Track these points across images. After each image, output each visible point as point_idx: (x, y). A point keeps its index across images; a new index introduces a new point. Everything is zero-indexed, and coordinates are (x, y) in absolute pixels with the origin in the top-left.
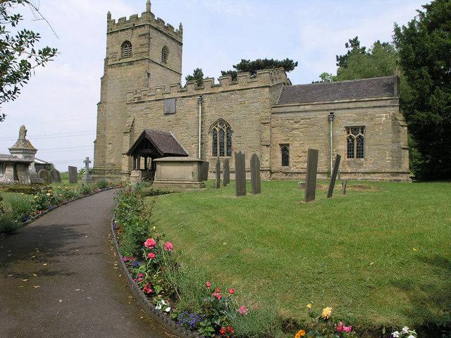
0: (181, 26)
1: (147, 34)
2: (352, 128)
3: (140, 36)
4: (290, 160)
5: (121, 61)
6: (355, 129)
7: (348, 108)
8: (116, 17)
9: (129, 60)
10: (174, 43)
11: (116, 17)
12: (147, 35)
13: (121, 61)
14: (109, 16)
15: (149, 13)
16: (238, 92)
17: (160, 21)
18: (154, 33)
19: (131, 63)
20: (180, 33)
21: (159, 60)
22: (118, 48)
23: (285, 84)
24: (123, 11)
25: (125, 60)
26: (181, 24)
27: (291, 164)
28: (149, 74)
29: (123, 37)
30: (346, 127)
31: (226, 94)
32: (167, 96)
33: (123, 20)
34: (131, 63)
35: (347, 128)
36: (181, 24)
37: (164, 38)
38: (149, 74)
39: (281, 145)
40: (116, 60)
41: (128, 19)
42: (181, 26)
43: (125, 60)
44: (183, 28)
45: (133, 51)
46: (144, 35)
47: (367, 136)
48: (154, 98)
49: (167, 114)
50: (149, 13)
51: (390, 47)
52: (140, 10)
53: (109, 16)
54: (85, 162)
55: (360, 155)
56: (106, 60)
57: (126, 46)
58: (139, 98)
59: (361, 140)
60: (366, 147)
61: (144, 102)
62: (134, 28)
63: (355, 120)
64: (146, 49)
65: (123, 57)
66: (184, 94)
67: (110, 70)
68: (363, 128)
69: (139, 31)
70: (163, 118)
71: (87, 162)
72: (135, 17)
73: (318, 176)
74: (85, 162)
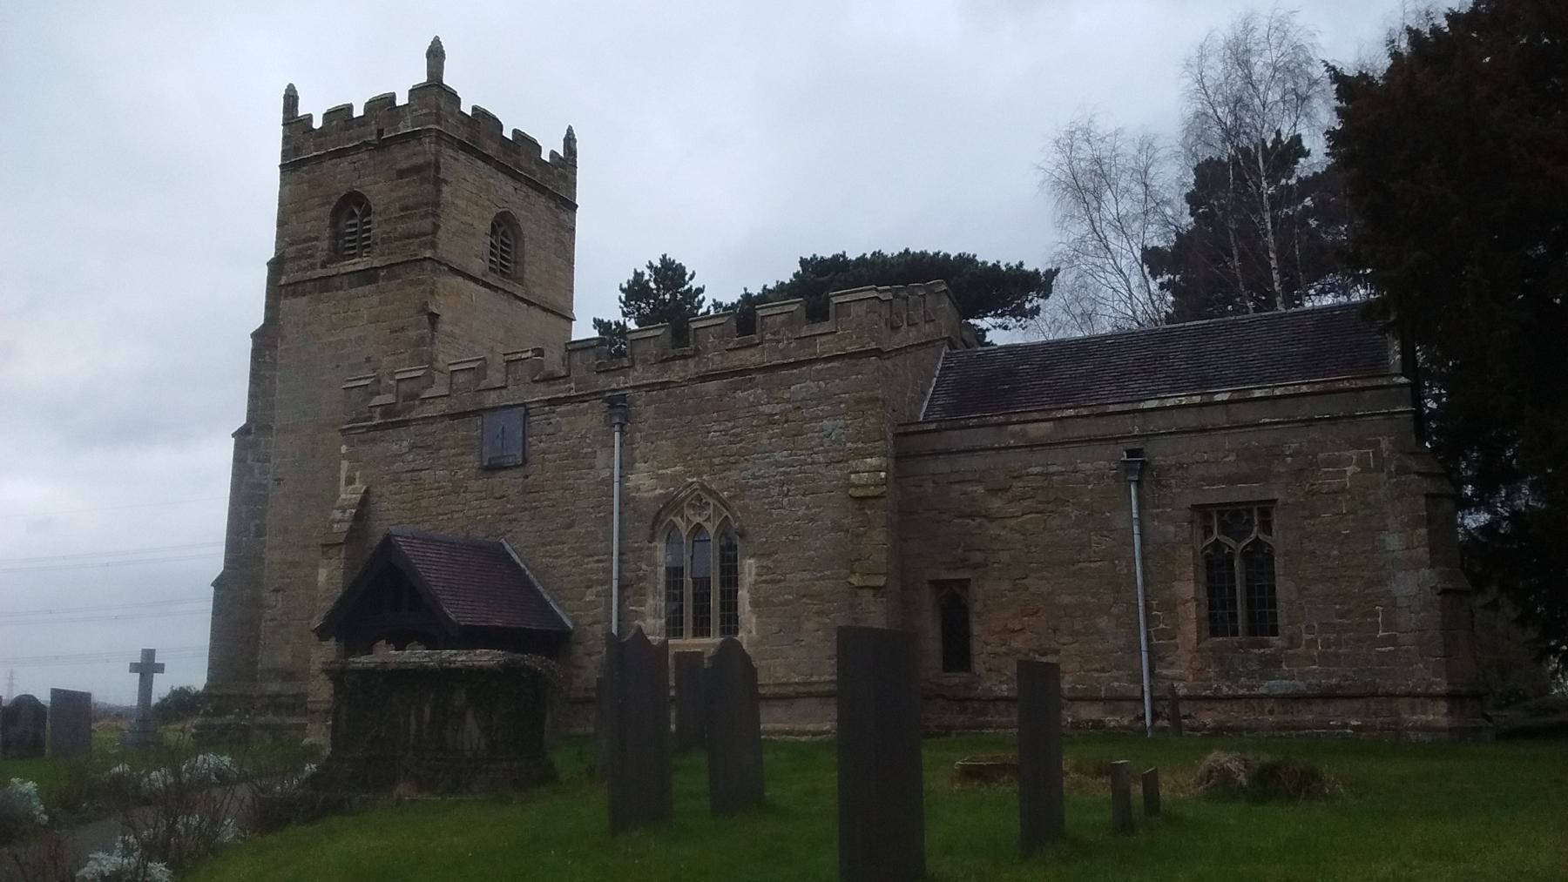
0: (570, 140)
1: (428, 165)
2: (1221, 508)
3: (402, 174)
4: (976, 647)
5: (332, 270)
6: (1233, 517)
7: (1202, 430)
8: (314, 107)
9: (361, 264)
10: (541, 201)
11: (314, 107)
12: (430, 173)
13: (332, 270)
14: (291, 99)
15: (434, 92)
16: (759, 377)
17: (484, 121)
18: (458, 167)
19: (368, 276)
20: (567, 162)
21: (477, 266)
22: (318, 220)
23: (952, 346)
24: (343, 82)
25: (348, 266)
26: (570, 130)
27: (978, 666)
28: (434, 318)
29: (342, 177)
30: (1194, 507)
31: (712, 386)
32: (492, 399)
33: (341, 115)
34: (368, 276)
35: (1203, 512)
36: (570, 130)
37: (505, 185)
38: (434, 318)
39: (937, 584)
40: (312, 267)
41: (358, 112)
42: (570, 140)
43: (348, 266)
44: (579, 147)
45: (377, 231)
46: (416, 169)
47: (1278, 539)
48: (442, 406)
49: (492, 468)
50: (434, 92)
51: (622, 328)
52: (402, 78)
53: (291, 99)
54: (135, 668)
55: (1263, 622)
56: (276, 266)
57: (353, 215)
58: (388, 410)
59: (1260, 560)
60: (1284, 588)
61: (405, 423)
62: (383, 145)
63: (1231, 480)
64: (426, 225)
65: (337, 254)
66: (559, 391)
67: (285, 304)
68: (1266, 509)
69: (402, 157)
70: (474, 485)
71: (147, 667)
72: (383, 105)
73: (773, 721)
74: (135, 668)
